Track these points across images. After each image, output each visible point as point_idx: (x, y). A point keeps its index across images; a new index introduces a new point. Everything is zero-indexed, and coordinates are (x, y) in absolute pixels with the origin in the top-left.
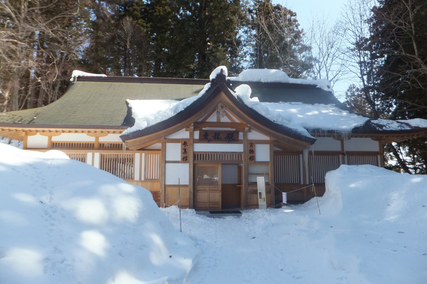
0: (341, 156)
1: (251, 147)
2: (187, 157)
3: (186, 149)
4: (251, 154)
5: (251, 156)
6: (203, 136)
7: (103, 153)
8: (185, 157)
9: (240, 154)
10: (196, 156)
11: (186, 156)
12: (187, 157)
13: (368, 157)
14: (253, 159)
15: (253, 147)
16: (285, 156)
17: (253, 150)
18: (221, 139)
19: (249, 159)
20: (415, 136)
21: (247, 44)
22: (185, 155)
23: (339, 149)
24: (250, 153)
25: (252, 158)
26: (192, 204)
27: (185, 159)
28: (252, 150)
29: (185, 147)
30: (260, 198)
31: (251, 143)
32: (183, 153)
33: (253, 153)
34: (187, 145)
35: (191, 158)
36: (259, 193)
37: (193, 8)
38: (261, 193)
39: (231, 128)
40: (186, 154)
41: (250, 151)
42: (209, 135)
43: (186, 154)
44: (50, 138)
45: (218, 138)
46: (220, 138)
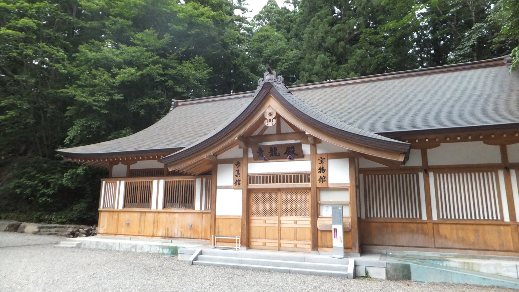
0: (421, 175)
1: (321, 164)
2: (240, 180)
3: (239, 170)
4: (322, 173)
5: (321, 177)
6: (257, 153)
7: (128, 181)
8: (238, 180)
9: (126, 183)
10: (251, 179)
11: (239, 180)
12: (240, 180)
13: (489, 174)
14: (325, 181)
15: (324, 163)
16: (370, 176)
17: (324, 168)
18: (279, 155)
19: (319, 180)
20: (75, 71)
21: (390, 45)
22: (237, 179)
23: (497, 159)
24: (320, 172)
25: (324, 179)
26: (245, 240)
27: (237, 183)
28: (323, 167)
29: (238, 168)
30: (334, 238)
31: (322, 158)
32: (236, 176)
33: (324, 173)
34: (240, 166)
35: (243, 182)
36: (334, 229)
37: (410, 39)
38: (336, 229)
39: (295, 140)
40: (239, 176)
41: (319, 169)
42: (263, 151)
43: (239, 176)
44: (129, 167)
45: (276, 155)
46: (278, 154)
